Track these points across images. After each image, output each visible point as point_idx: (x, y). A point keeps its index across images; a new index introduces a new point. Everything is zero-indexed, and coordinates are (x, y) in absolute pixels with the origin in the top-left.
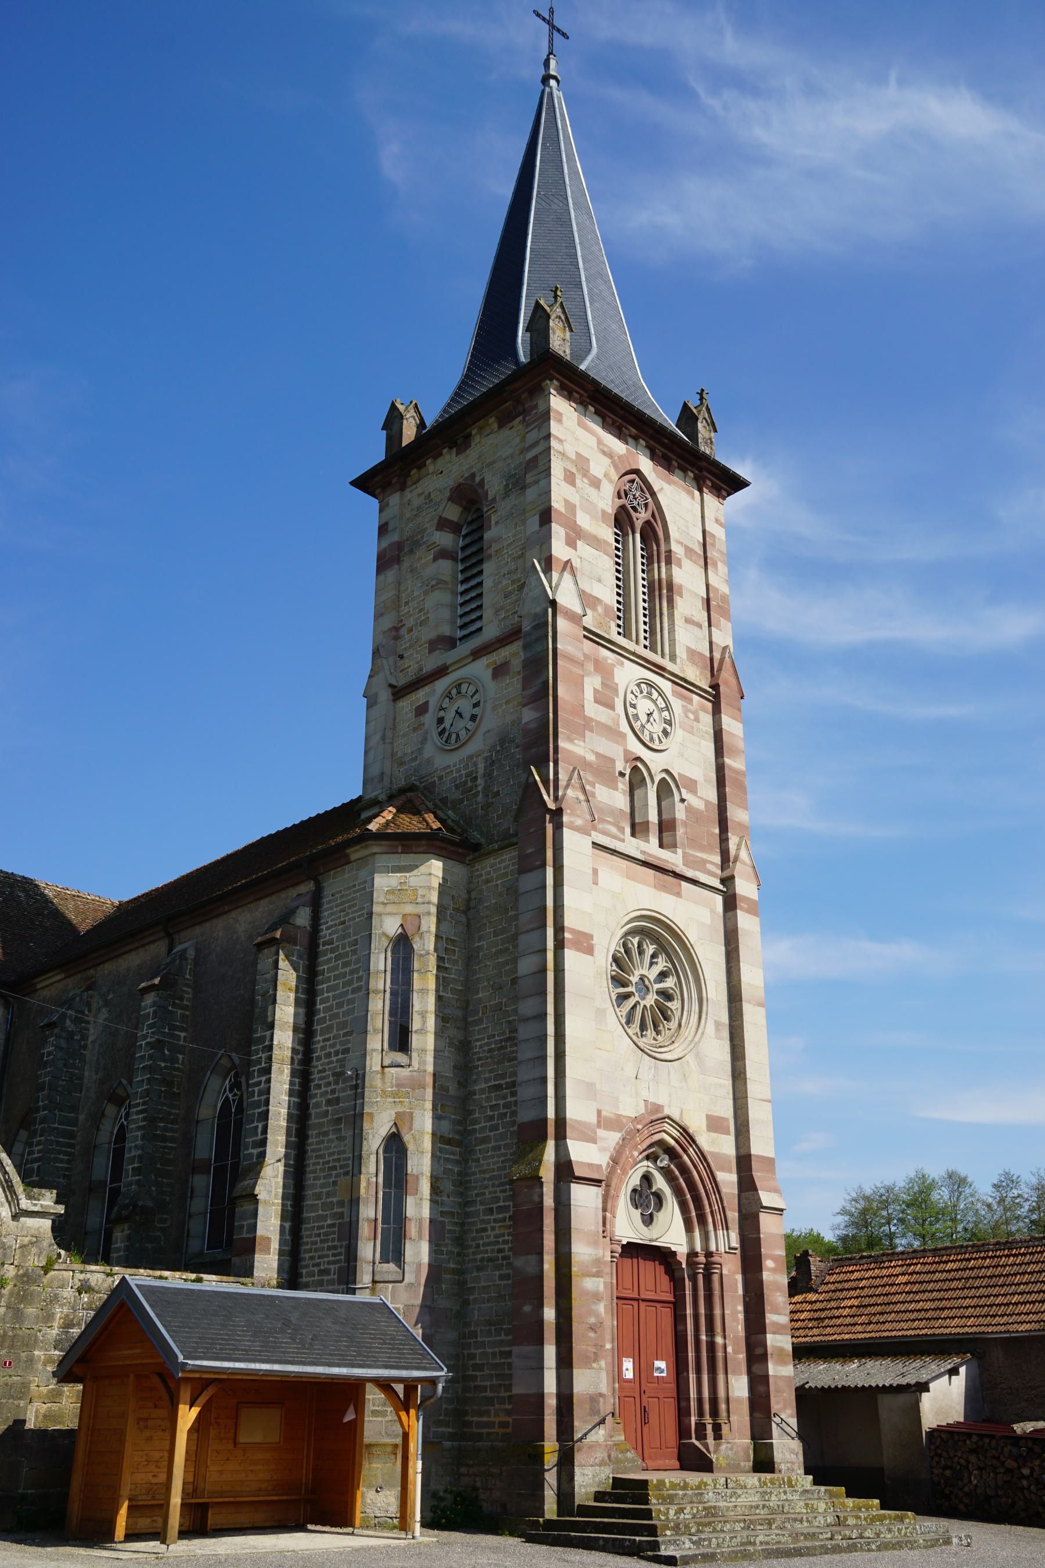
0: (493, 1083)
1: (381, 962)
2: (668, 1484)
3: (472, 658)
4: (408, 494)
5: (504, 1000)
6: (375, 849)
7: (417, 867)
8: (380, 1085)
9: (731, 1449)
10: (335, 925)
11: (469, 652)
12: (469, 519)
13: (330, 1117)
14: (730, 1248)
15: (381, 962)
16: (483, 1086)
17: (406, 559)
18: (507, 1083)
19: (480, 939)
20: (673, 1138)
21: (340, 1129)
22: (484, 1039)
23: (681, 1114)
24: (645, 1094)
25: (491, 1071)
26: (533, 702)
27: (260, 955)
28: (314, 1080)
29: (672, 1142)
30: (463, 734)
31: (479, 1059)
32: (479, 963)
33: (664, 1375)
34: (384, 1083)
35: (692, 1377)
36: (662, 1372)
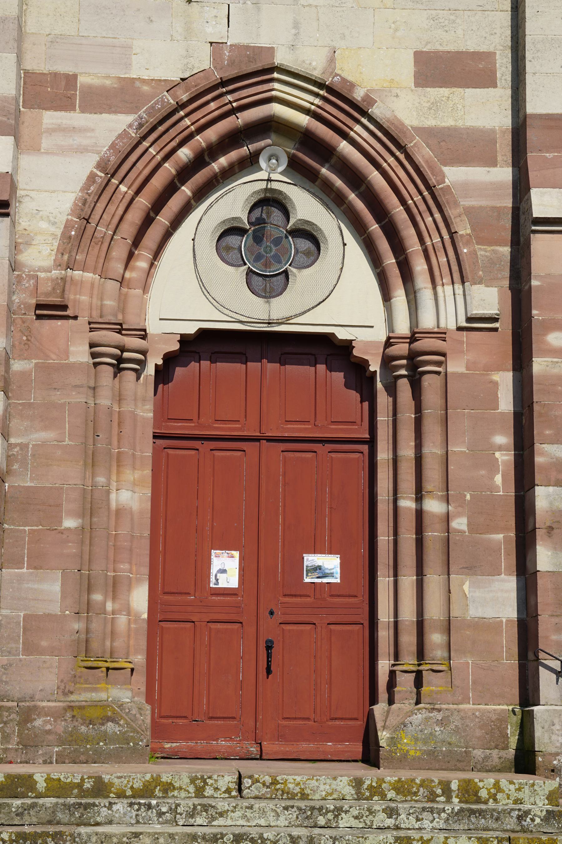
2: (41, 785)
9: (441, 723)
14: (469, 320)
20: (307, 112)
23: (332, 60)
24: (216, 31)
29: (303, 120)
33: (336, 579)
35: (384, 583)
36: (331, 575)
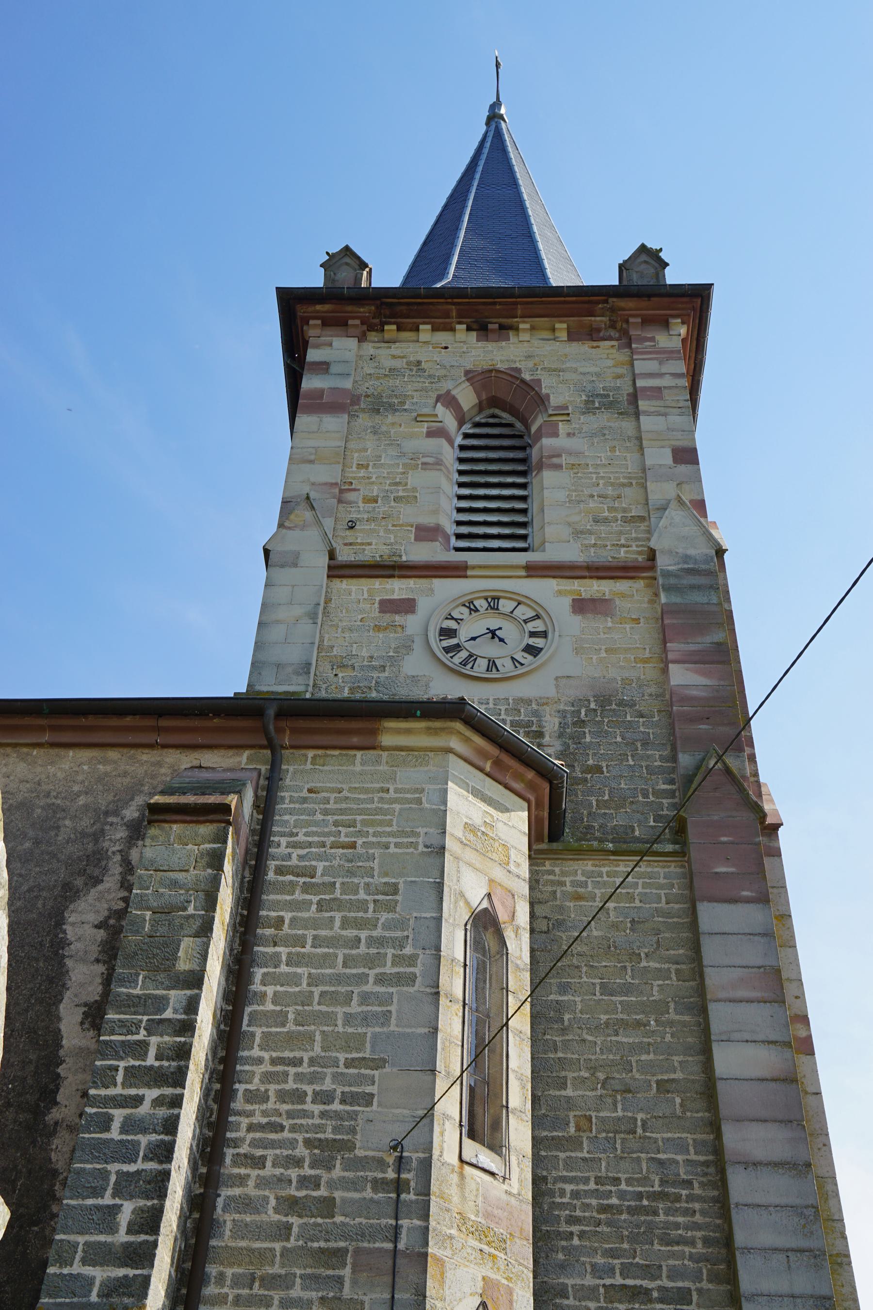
0: (619, 1280)
1: (455, 943)
3: (523, 573)
4: (369, 348)
5: (640, 1116)
6: (455, 743)
7: (507, 810)
8: (456, 1199)
10: (310, 845)
11: (523, 563)
12: (477, 419)
13: (292, 1243)
15: (455, 943)
16: (589, 1281)
17: (523, 375)
18: (660, 1289)
19: (564, 989)
21: (340, 1280)
22: (586, 1181)
25: (612, 1254)
26: (695, 663)
27: (153, 831)
28: (236, 1143)
30: (481, 665)
31: (573, 1220)
32: (564, 1031)
34: (463, 1197)
